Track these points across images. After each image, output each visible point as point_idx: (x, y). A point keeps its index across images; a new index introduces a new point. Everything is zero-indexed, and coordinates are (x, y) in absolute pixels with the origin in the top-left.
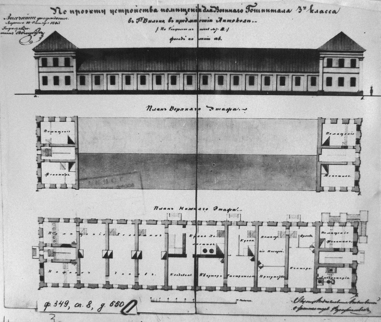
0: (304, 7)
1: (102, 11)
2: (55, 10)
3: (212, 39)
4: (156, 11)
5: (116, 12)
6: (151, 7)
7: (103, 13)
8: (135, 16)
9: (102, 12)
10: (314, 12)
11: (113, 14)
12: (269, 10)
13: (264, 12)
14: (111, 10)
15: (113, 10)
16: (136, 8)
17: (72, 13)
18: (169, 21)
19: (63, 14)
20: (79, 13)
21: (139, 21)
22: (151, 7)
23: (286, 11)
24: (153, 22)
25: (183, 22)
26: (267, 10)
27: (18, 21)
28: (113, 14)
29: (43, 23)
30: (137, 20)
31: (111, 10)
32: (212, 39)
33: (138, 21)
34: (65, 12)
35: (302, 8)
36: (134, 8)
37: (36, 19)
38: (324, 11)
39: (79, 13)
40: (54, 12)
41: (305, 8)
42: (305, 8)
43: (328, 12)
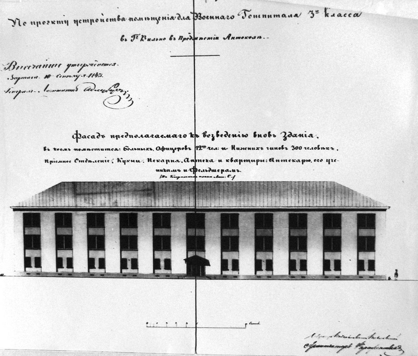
0: (316, 11)
1: (65, 21)
2: (15, 23)
3: (108, 137)
4: (123, 19)
5: (80, 22)
6: (119, 16)
7: (76, 24)
8: (129, 29)
9: (65, 23)
10: (330, 15)
11: (77, 25)
12: (213, 17)
13: (265, 17)
14: (75, 21)
15: (77, 20)
16: (102, 18)
17: (217, 18)
18: (171, 39)
19: (343, 17)
20: (40, 24)
21: (134, 39)
22: (119, 16)
23: (293, 16)
24: (253, 38)
25: (187, 40)
26: (211, 17)
27: (32, 72)
28: (77, 25)
29: (74, 76)
30: (132, 37)
31: (75, 21)
32: (108, 137)
33: (133, 39)
34: (250, 17)
35: (314, 12)
36: (100, 17)
37: (64, 67)
38: (343, 15)
39: (93, 22)
40: (13, 24)
41: (317, 11)
42: (317, 11)
43: (347, 15)
